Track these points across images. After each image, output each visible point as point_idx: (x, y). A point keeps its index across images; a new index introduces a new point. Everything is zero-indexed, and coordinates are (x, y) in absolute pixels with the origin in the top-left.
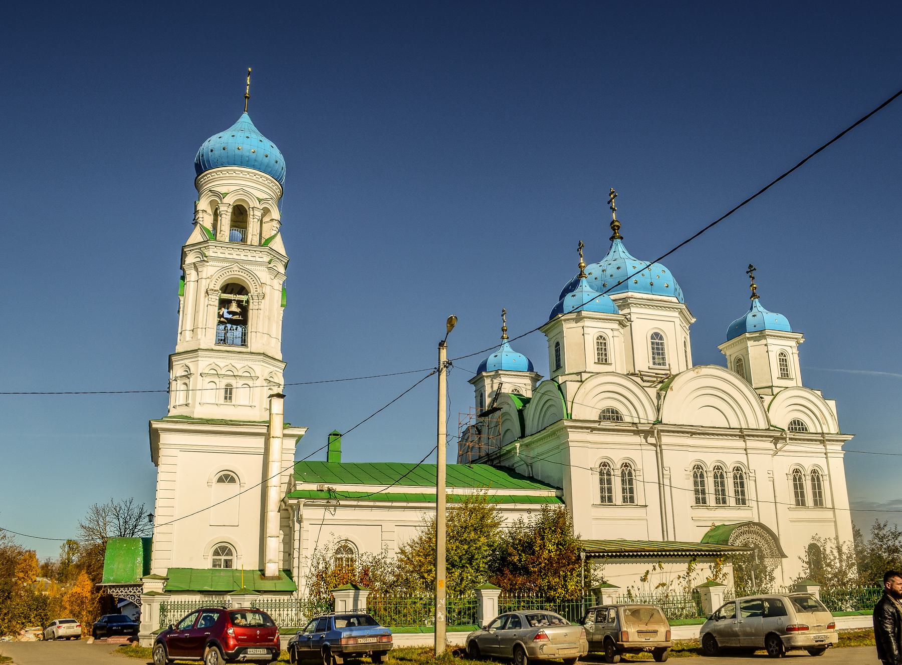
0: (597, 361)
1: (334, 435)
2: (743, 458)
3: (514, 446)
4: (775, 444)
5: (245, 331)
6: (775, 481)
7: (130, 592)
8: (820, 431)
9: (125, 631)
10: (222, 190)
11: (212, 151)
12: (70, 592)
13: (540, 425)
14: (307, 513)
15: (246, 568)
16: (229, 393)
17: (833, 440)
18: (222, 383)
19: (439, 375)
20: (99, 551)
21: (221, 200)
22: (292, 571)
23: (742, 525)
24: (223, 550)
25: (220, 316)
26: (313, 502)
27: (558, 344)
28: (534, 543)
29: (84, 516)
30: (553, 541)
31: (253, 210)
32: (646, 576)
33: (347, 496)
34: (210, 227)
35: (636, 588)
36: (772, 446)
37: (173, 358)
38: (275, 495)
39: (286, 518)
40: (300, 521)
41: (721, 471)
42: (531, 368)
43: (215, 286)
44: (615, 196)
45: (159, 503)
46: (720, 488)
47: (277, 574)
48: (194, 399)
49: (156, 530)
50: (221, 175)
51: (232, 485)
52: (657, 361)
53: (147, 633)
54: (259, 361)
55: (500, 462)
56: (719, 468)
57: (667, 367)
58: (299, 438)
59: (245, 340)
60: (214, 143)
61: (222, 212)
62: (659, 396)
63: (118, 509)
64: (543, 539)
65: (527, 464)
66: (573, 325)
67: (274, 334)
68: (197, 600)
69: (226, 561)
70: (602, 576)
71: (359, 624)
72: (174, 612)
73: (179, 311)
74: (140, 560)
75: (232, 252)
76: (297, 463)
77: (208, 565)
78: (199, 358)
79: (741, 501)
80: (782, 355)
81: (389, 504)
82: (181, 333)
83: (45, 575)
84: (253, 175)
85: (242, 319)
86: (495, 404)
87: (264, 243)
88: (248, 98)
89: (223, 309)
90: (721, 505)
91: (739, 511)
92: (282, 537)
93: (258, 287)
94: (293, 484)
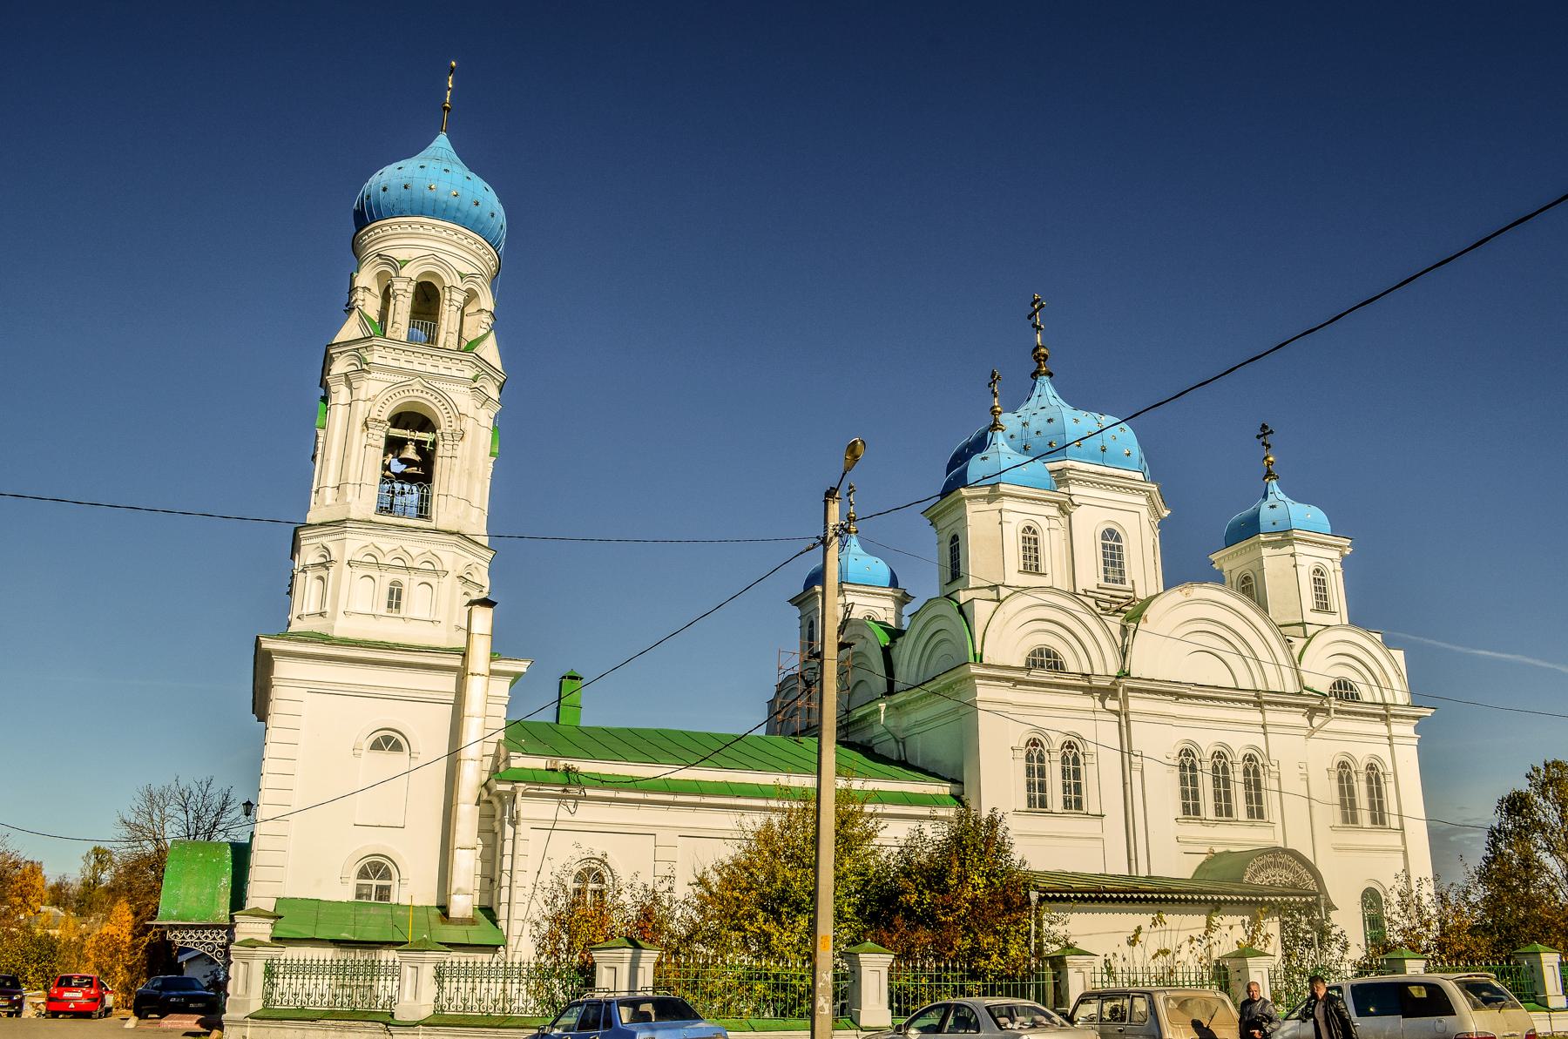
0: (1022, 569)
1: (570, 678)
2: (1259, 741)
3: (875, 707)
4: (1310, 719)
5: (428, 492)
6: (1310, 779)
7: (207, 937)
8: (1379, 700)
9: (192, 1005)
10: (400, 255)
11: (385, 189)
12: (98, 932)
13: (921, 674)
14: (528, 808)
15: (417, 903)
16: (395, 597)
17: (1401, 716)
18: (390, 577)
19: (825, 551)
20: (157, 863)
21: (397, 272)
22: (495, 910)
23: (1263, 854)
24: (376, 869)
25: (386, 467)
26: (539, 789)
27: (955, 538)
28: (946, 871)
29: (128, 804)
30: (981, 868)
31: (450, 292)
32: (1136, 936)
33: (602, 781)
34: (375, 316)
35: (1120, 958)
36: (1305, 721)
37: (302, 534)
38: (471, 776)
39: (488, 816)
40: (514, 823)
41: (1223, 760)
42: (894, 583)
43: (380, 413)
44: (1042, 306)
45: (266, 781)
46: (1222, 789)
47: (470, 914)
48: (335, 606)
49: (260, 829)
50: (399, 230)
51: (395, 755)
52: (1110, 576)
53: (240, 1015)
54: (451, 545)
55: (847, 736)
56: (1220, 755)
57: (1128, 586)
58: (517, 676)
59: (427, 508)
60: (390, 177)
61: (398, 292)
62: (1124, 631)
63: (186, 795)
64: (963, 864)
65: (895, 739)
66: (984, 506)
67: (476, 501)
68: (328, 959)
69: (381, 889)
70: (1065, 933)
71: (660, 1016)
72: (291, 978)
73: (314, 457)
74: (226, 881)
75: (412, 358)
76: (511, 725)
77: (348, 895)
78: (347, 535)
79: (1256, 811)
80: (1318, 572)
81: (670, 798)
82: (317, 492)
83: (56, 903)
84: (453, 233)
85: (422, 472)
86: (841, 636)
87: (468, 347)
88: (449, 110)
89: (391, 456)
90: (1224, 818)
91: (1253, 830)
92: (480, 849)
93: (453, 419)
94: (503, 756)
